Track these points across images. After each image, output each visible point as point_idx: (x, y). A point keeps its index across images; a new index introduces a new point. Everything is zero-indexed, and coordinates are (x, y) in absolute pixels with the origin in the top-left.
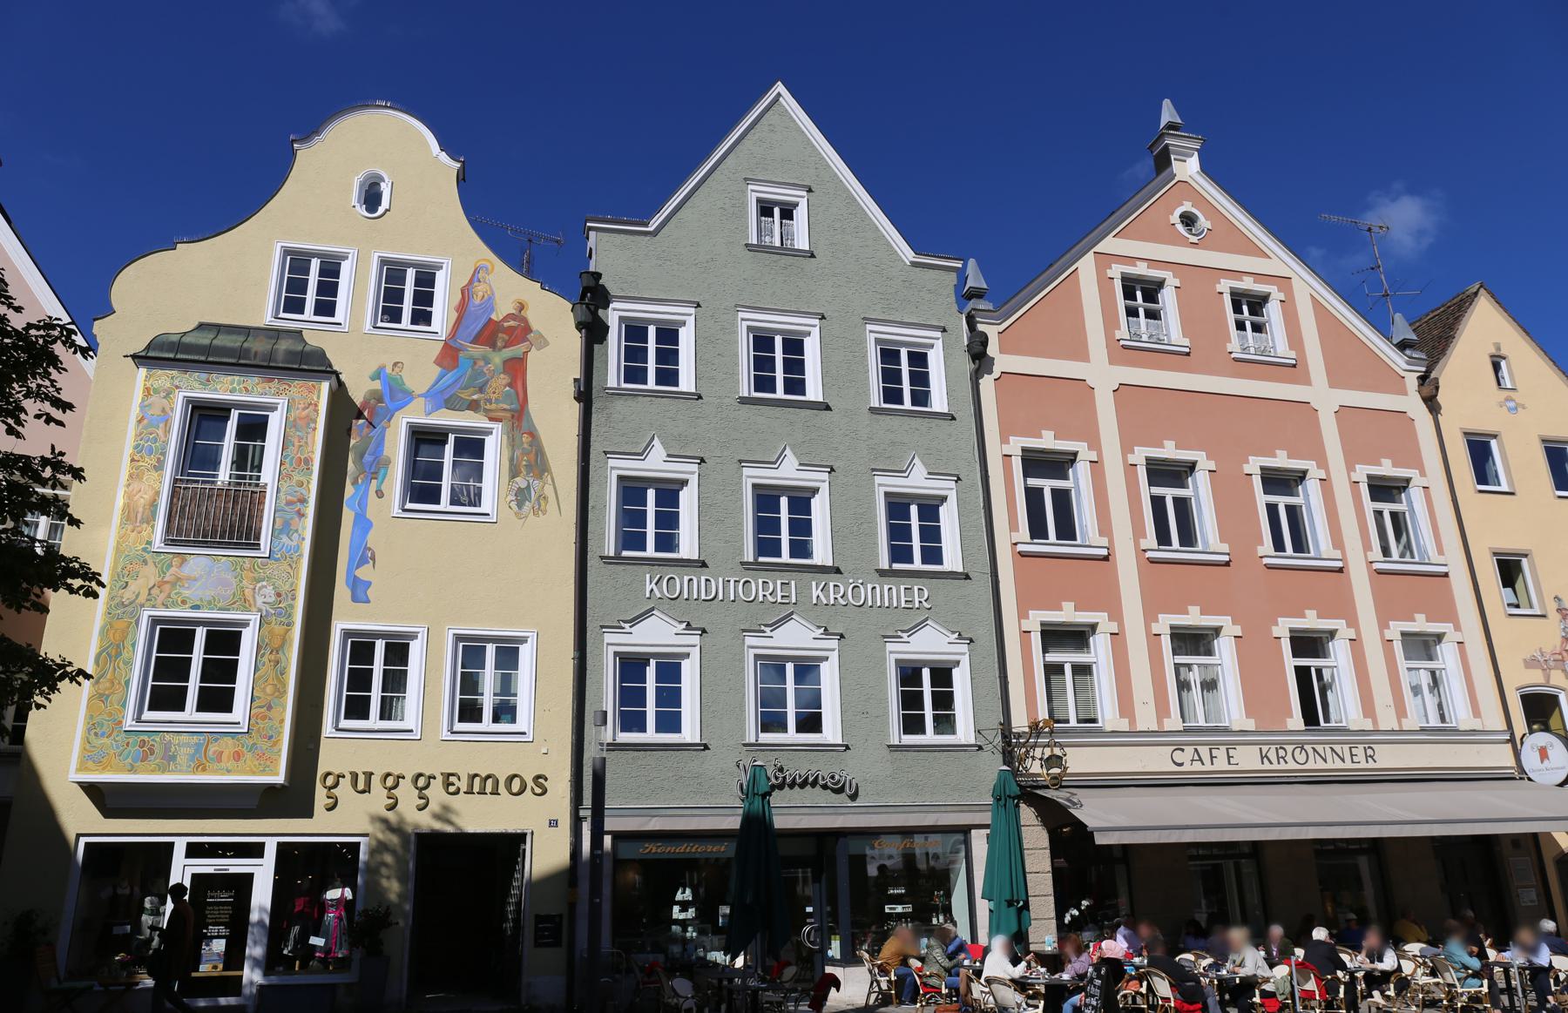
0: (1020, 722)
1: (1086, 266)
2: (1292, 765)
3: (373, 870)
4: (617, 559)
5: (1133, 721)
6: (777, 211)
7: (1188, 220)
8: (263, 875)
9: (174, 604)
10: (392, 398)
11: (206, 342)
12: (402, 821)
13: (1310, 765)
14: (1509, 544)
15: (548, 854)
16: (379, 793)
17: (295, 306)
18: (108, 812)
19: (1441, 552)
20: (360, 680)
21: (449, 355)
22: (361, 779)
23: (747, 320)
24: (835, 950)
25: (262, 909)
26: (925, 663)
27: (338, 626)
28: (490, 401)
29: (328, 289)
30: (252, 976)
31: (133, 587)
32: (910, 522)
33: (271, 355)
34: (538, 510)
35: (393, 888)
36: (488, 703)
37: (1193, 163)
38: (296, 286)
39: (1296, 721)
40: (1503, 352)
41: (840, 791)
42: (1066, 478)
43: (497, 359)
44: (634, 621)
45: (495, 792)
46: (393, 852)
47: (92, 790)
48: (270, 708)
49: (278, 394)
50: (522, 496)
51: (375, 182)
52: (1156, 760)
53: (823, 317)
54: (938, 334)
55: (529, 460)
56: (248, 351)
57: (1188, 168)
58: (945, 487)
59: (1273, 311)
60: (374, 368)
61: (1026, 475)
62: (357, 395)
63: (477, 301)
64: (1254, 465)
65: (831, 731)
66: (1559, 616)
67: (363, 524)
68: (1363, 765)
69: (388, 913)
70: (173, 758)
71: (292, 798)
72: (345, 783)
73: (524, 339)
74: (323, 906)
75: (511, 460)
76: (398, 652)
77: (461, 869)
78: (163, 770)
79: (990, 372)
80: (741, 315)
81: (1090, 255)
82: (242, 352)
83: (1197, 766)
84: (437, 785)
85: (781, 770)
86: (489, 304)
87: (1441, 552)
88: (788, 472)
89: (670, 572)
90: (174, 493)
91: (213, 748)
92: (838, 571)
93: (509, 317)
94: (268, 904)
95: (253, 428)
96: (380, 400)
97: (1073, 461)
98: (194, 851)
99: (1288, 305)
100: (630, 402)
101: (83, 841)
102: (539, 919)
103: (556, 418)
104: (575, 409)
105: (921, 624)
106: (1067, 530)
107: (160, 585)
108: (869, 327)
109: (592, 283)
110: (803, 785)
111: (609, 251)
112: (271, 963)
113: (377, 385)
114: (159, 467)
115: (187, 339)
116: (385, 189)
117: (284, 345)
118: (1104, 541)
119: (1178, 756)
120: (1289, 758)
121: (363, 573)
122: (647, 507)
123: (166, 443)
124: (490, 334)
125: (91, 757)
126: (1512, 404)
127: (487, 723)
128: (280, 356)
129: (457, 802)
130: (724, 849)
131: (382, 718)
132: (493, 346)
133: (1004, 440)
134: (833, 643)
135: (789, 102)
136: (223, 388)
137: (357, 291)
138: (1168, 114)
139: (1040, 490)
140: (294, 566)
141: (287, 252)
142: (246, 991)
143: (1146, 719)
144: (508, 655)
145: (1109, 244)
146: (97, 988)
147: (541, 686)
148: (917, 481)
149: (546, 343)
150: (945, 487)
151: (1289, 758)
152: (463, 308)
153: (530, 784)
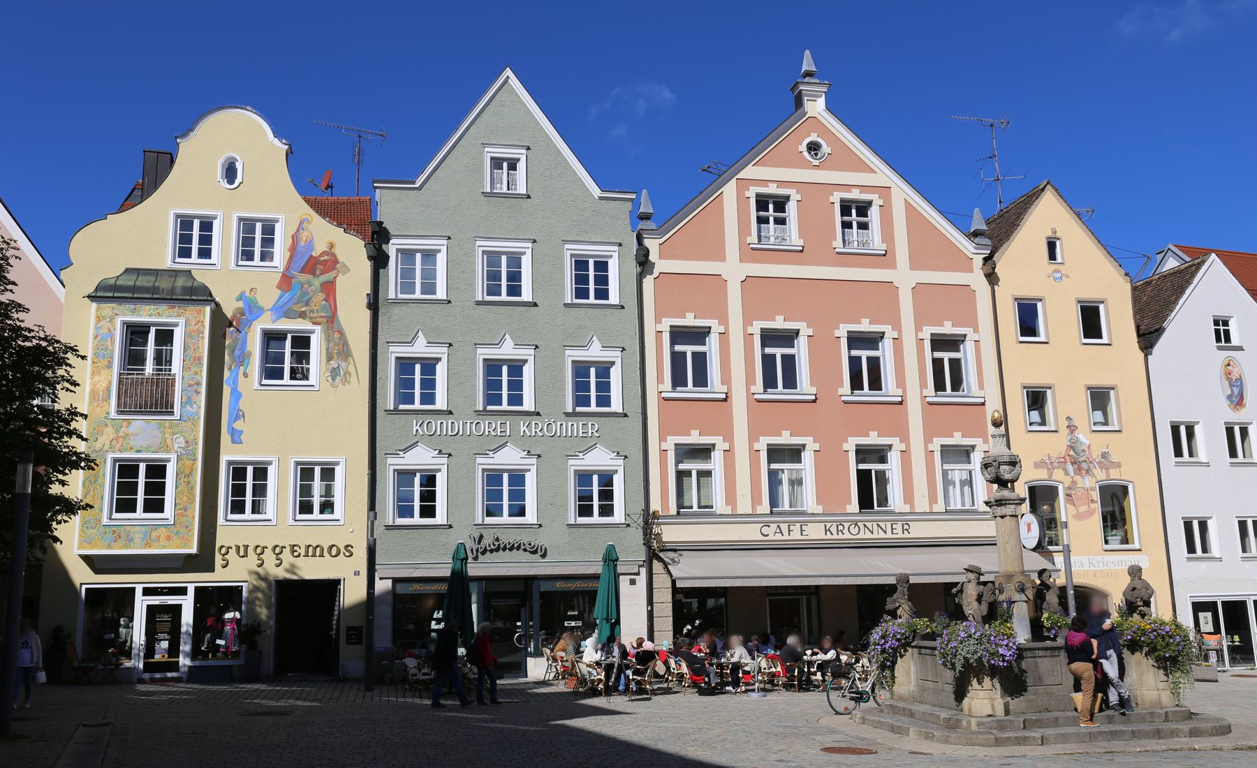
0: (655, 505)
1: (729, 190)
2: (847, 536)
3: (251, 602)
4: (396, 411)
5: (912, 506)
6: (505, 165)
7: (814, 148)
8: (187, 605)
9: (126, 450)
10: (250, 312)
11: (132, 283)
12: (267, 573)
13: (861, 536)
14: (1036, 380)
15: (353, 593)
16: (252, 559)
17: (185, 253)
18: (97, 571)
19: (981, 387)
20: (239, 490)
21: (286, 282)
22: (242, 549)
23: (570, 249)
24: (531, 649)
25: (188, 625)
26: (595, 472)
27: (224, 459)
28: (312, 311)
29: (206, 240)
30: (184, 661)
31: (101, 440)
32: (589, 382)
33: (172, 291)
34: (345, 381)
35: (263, 612)
36: (317, 501)
37: (821, 102)
38: (185, 239)
39: (854, 506)
40: (1058, 235)
41: (535, 552)
42: (958, 351)
43: (317, 282)
44: (406, 450)
45: (322, 555)
46: (263, 592)
47: (87, 559)
48: (186, 510)
49: (179, 316)
50: (334, 373)
51: (234, 162)
52: (750, 533)
53: (535, 241)
54: (616, 248)
55: (339, 350)
56: (158, 288)
57: (816, 107)
58: (614, 355)
59: (874, 214)
60: (238, 293)
61: (933, 350)
62: (229, 312)
63: (303, 244)
64: (842, 331)
65: (531, 517)
66: (1068, 431)
67: (236, 395)
68: (900, 535)
69: (259, 626)
70: (132, 540)
71: (203, 561)
72: (233, 552)
73: (334, 268)
74: (223, 623)
75: (327, 350)
76: (261, 473)
77: (305, 601)
78: (127, 547)
79: (651, 273)
80: (478, 243)
81: (734, 181)
82: (154, 290)
83: (779, 537)
84: (287, 551)
85: (497, 540)
86: (310, 245)
87: (981, 387)
88: (508, 350)
89: (428, 418)
90: (120, 382)
91: (154, 534)
92: (538, 414)
93: (324, 253)
94: (191, 622)
95: (165, 337)
96: (243, 314)
97: (882, 337)
98: (147, 592)
99: (886, 209)
100: (404, 307)
101: (84, 587)
102: (349, 629)
103: (355, 320)
104: (367, 315)
105: (593, 447)
106: (876, 384)
107: (116, 439)
108: (567, 246)
109: (377, 229)
110: (511, 549)
111: (390, 205)
112: (195, 653)
113: (240, 304)
114: (110, 366)
115: (120, 282)
116: (239, 166)
117: (181, 282)
118: (900, 392)
119: (765, 530)
120: (846, 531)
121: (238, 425)
122: (415, 375)
123: (113, 351)
124: (311, 266)
125: (85, 541)
126: (1058, 275)
127: (316, 514)
128: (178, 291)
129: (299, 562)
130: (444, 587)
131: (253, 512)
132: (314, 274)
133: (658, 320)
134: (534, 461)
135: (515, 82)
136: (146, 314)
137: (225, 239)
138: (808, 64)
139: (942, 360)
140: (195, 424)
141: (241, 219)
142: (182, 670)
143: (744, 506)
144: (328, 474)
145: (749, 172)
146: (100, 667)
147: (348, 490)
148: (595, 352)
149: (349, 270)
150: (614, 355)
151: (846, 531)
152: (293, 249)
153: (343, 550)
